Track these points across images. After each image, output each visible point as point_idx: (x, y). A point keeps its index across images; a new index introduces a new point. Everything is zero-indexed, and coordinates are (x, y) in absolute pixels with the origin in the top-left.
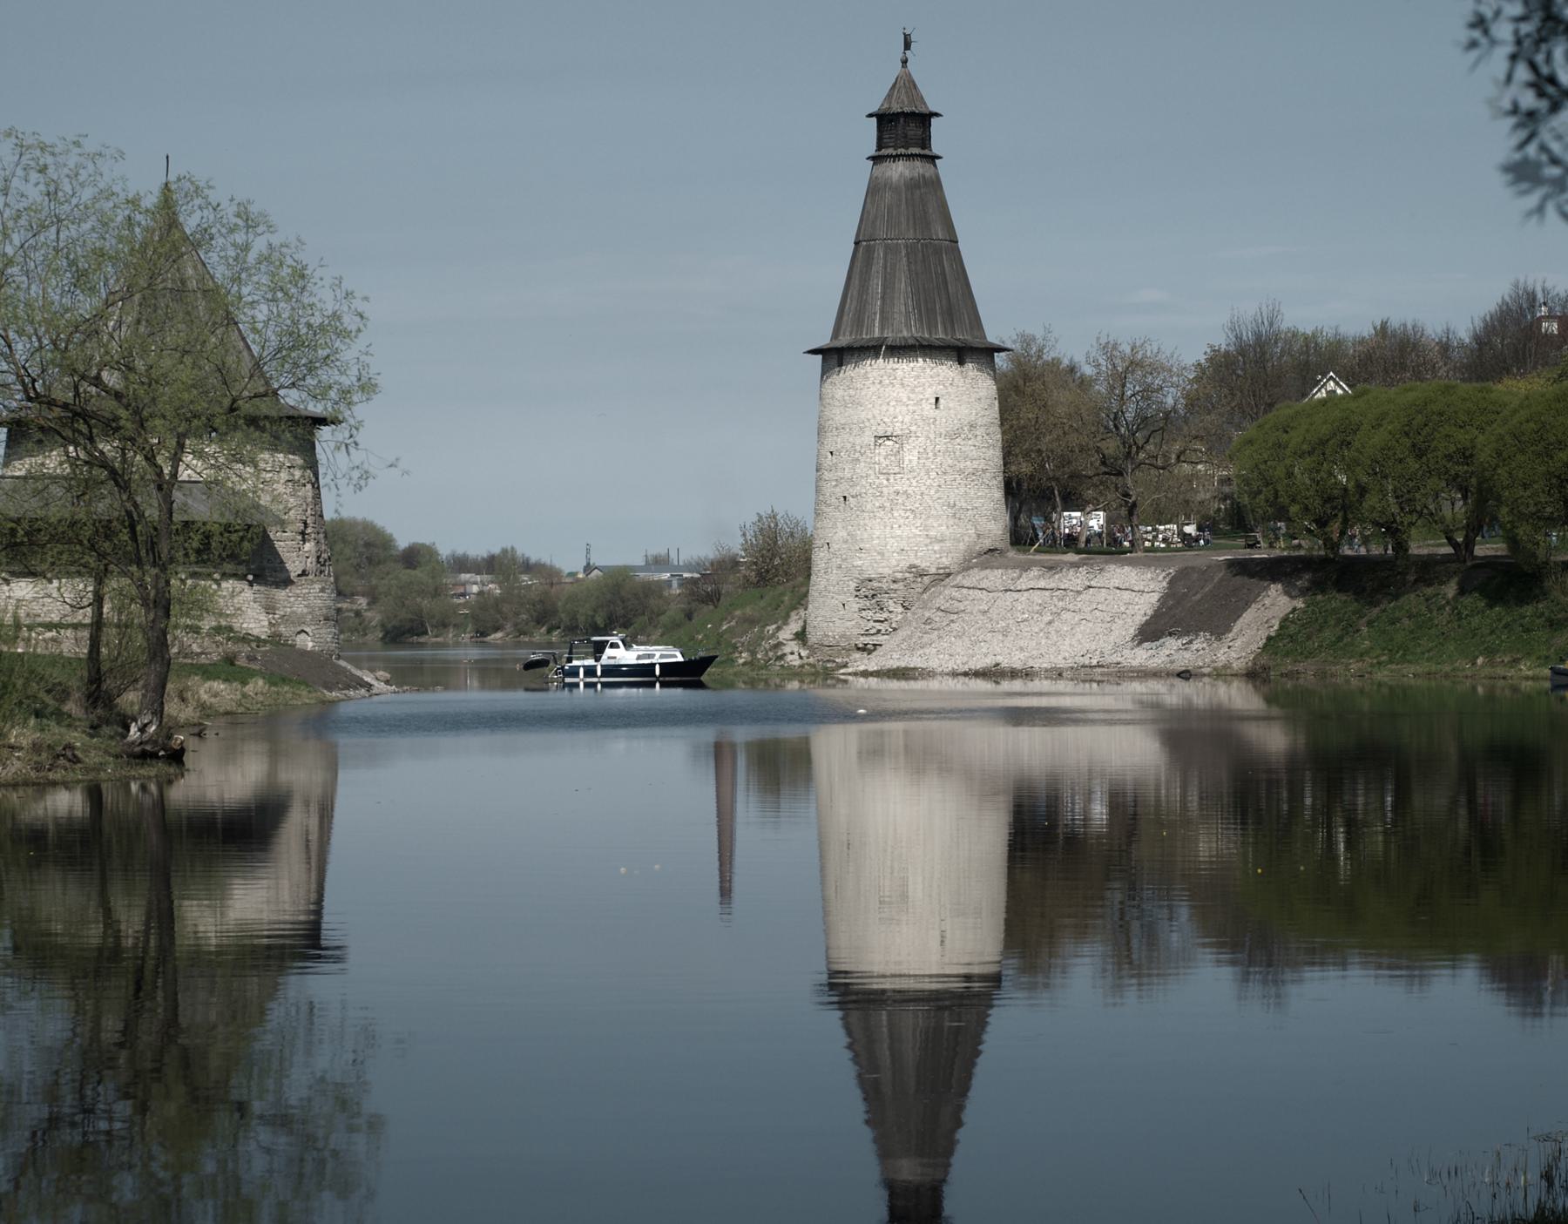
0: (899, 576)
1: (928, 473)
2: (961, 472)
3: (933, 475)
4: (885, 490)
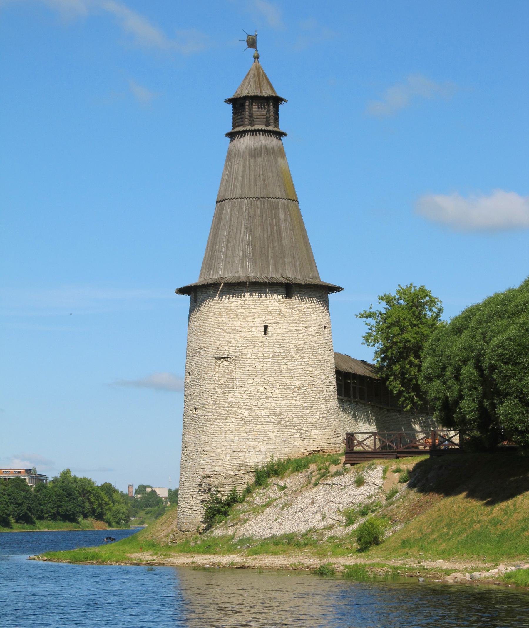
0: (231, 473)
1: (256, 387)
3: (261, 389)
4: (222, 402)
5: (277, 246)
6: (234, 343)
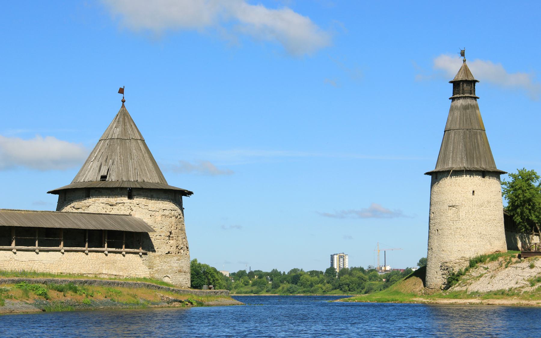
0: (458, 261)
1: (469, 220)
2: (483, 220)
3: (472, 221)
5: (477, 153)
6: (458, 199)
